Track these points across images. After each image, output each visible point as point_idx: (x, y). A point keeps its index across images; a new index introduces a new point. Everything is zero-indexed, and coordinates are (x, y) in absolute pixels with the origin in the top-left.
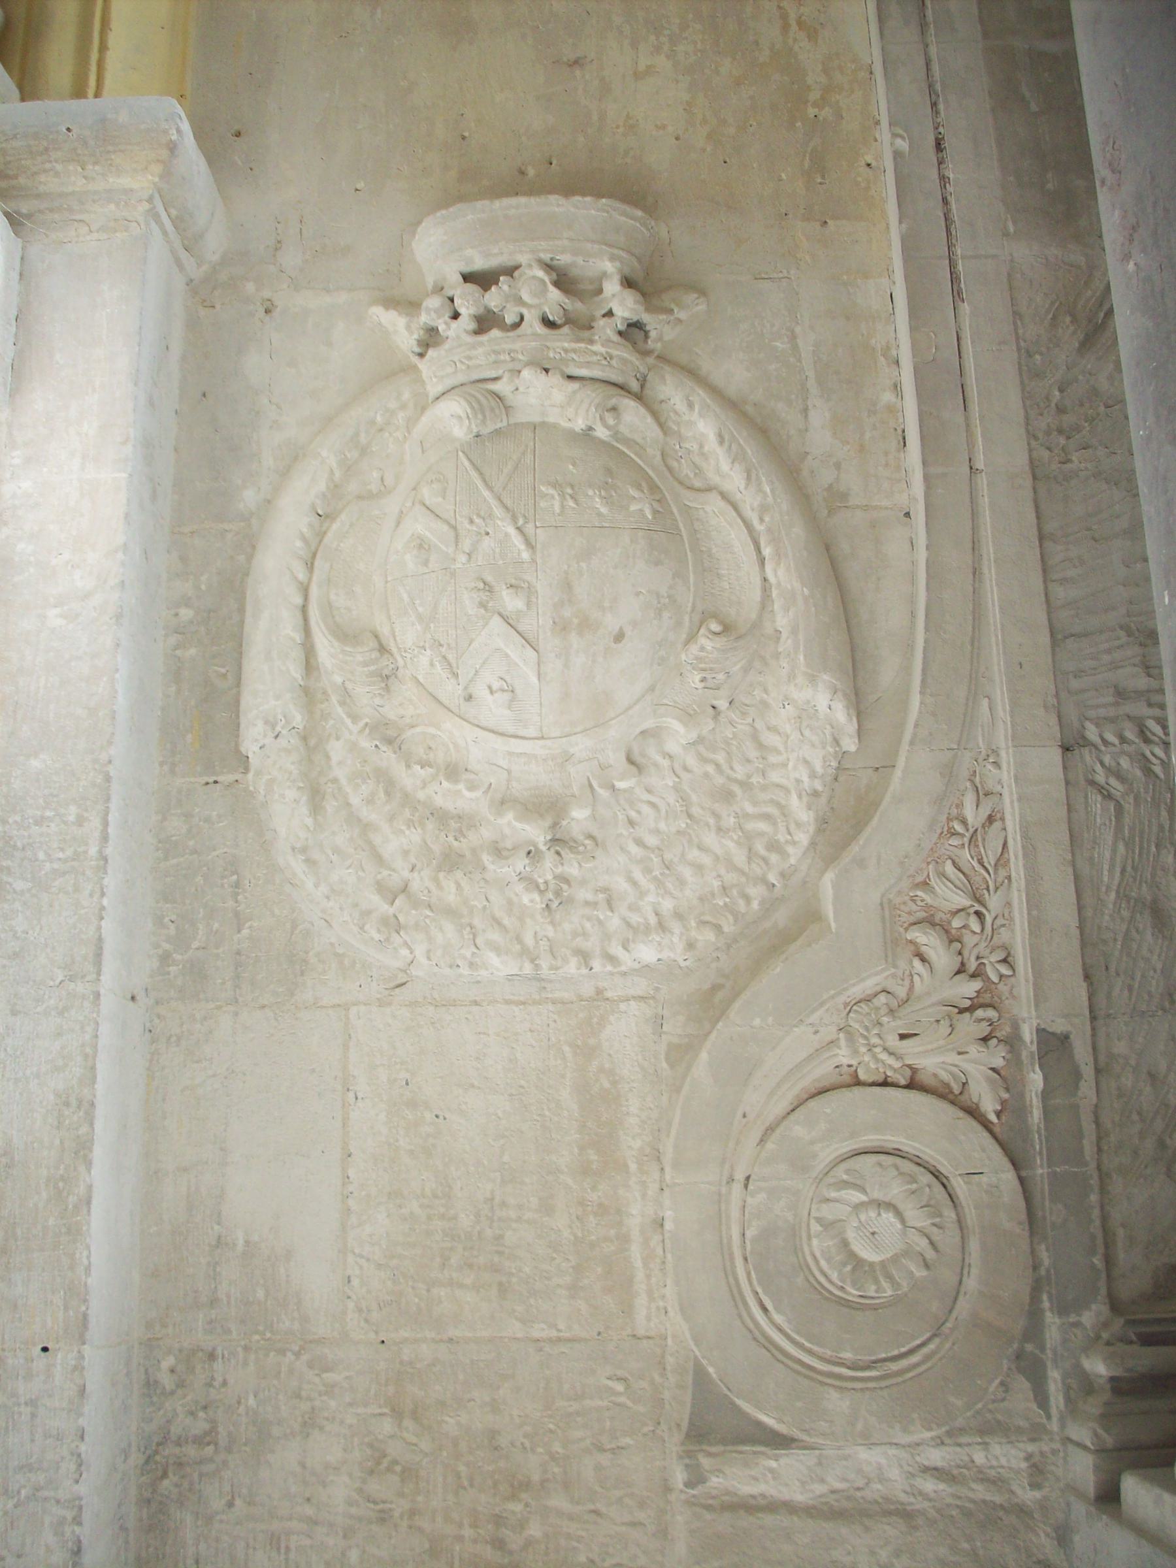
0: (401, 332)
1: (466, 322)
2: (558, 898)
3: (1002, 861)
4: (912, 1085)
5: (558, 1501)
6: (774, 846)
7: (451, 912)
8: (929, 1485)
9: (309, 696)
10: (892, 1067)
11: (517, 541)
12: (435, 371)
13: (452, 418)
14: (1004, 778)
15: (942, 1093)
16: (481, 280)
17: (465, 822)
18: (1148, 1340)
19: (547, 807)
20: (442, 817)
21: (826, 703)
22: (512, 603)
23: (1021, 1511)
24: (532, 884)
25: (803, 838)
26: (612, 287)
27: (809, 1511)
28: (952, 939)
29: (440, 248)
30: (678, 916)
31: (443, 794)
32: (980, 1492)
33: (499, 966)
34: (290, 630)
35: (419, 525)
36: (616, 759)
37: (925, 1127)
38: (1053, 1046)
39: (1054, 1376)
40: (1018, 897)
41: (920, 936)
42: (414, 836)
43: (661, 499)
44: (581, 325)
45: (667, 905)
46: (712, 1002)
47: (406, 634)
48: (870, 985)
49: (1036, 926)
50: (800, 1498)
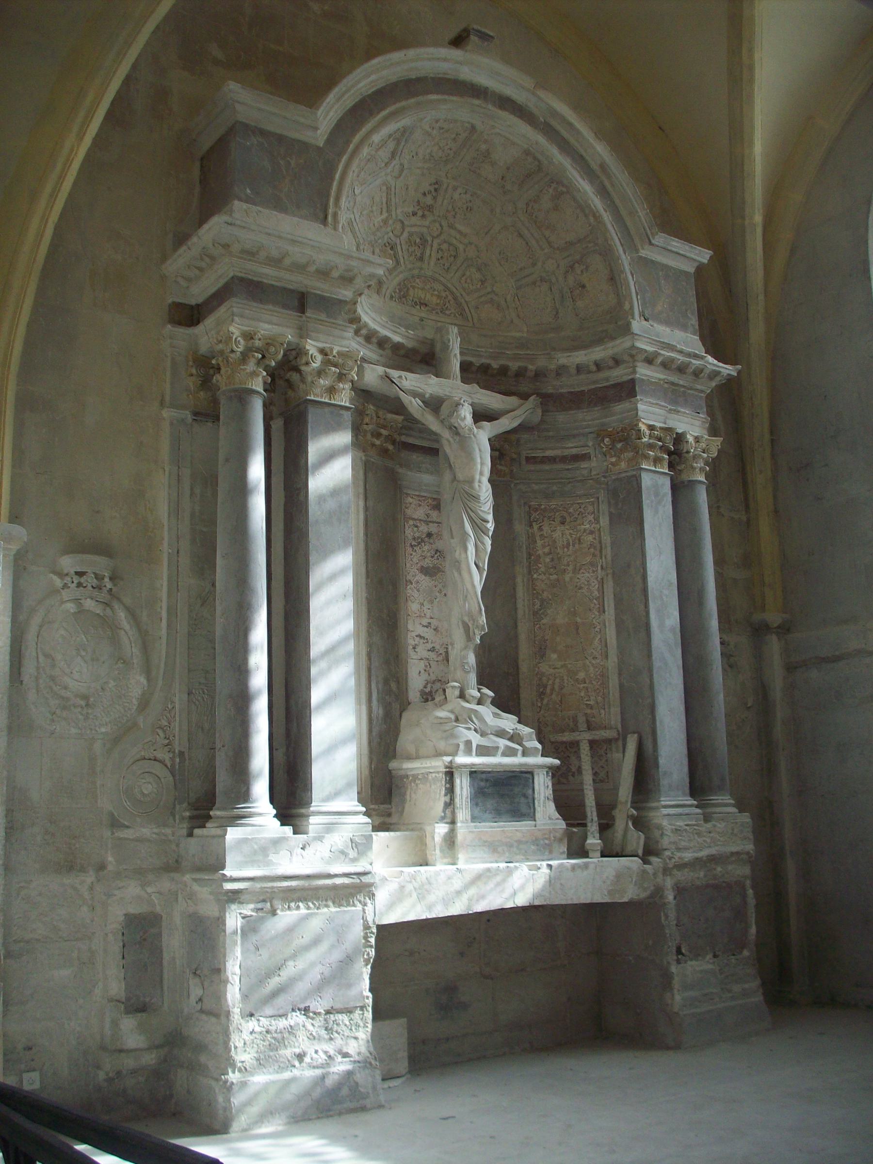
0: (58, 582)
1: (75, 585)
2: (86, 718)
3: (174, 717)
4: (155, 760)
5: (82, 840)
6: (129, 709)
7: (65, 719)
8: (154, 836)
9: (38, 668)
10: (151, 756)
11: (85, 639)
12: (65, 595)
13: (71, 607)
14: (177, 700)
15: (160, 761)
16: (80, 574)
17: (68, 699)
18: (195, 810)
19: (85, 697)
20: (63, 698)
21: (143, 680)
22: (83, 653)
23: (170, 841)
24: (82, 715)
25: (135, 707)
26: (107, 580)
27: (133, 840)
28: (164, 731)
29: (68, 563)
30: (110, 722)
31: (63, 693)
32: (163, 838)
33: (73, 731)
34: (34, 654)
35: (62, 632)
36: (99, 688)
37: (157, 768)
38: (181, 754)
39: (177, 817)
40: (177, 725)
41: (158, 730)
42: (57, 702)
43: (109, 625)
44: (99, 588)
45: (108, 720)
46: (116, 740)
47: (59, 657)
48: (149, 739)
49: (180, 730)
50: (131, 837)
